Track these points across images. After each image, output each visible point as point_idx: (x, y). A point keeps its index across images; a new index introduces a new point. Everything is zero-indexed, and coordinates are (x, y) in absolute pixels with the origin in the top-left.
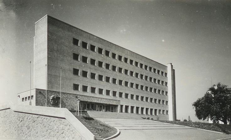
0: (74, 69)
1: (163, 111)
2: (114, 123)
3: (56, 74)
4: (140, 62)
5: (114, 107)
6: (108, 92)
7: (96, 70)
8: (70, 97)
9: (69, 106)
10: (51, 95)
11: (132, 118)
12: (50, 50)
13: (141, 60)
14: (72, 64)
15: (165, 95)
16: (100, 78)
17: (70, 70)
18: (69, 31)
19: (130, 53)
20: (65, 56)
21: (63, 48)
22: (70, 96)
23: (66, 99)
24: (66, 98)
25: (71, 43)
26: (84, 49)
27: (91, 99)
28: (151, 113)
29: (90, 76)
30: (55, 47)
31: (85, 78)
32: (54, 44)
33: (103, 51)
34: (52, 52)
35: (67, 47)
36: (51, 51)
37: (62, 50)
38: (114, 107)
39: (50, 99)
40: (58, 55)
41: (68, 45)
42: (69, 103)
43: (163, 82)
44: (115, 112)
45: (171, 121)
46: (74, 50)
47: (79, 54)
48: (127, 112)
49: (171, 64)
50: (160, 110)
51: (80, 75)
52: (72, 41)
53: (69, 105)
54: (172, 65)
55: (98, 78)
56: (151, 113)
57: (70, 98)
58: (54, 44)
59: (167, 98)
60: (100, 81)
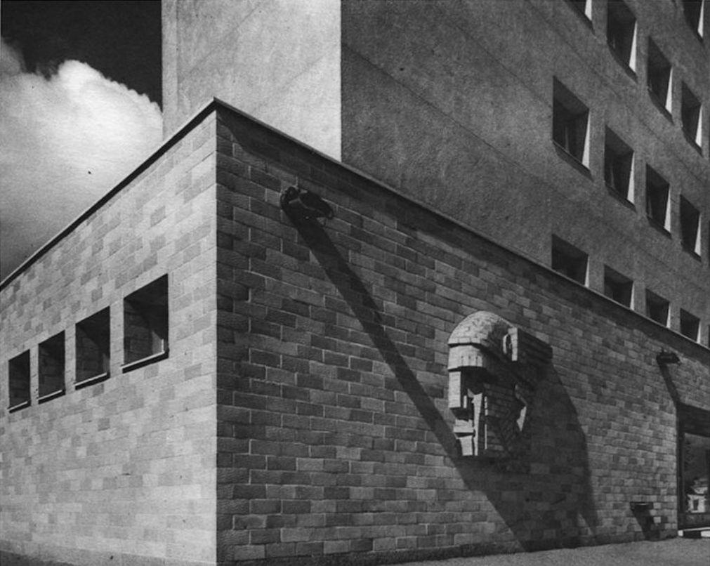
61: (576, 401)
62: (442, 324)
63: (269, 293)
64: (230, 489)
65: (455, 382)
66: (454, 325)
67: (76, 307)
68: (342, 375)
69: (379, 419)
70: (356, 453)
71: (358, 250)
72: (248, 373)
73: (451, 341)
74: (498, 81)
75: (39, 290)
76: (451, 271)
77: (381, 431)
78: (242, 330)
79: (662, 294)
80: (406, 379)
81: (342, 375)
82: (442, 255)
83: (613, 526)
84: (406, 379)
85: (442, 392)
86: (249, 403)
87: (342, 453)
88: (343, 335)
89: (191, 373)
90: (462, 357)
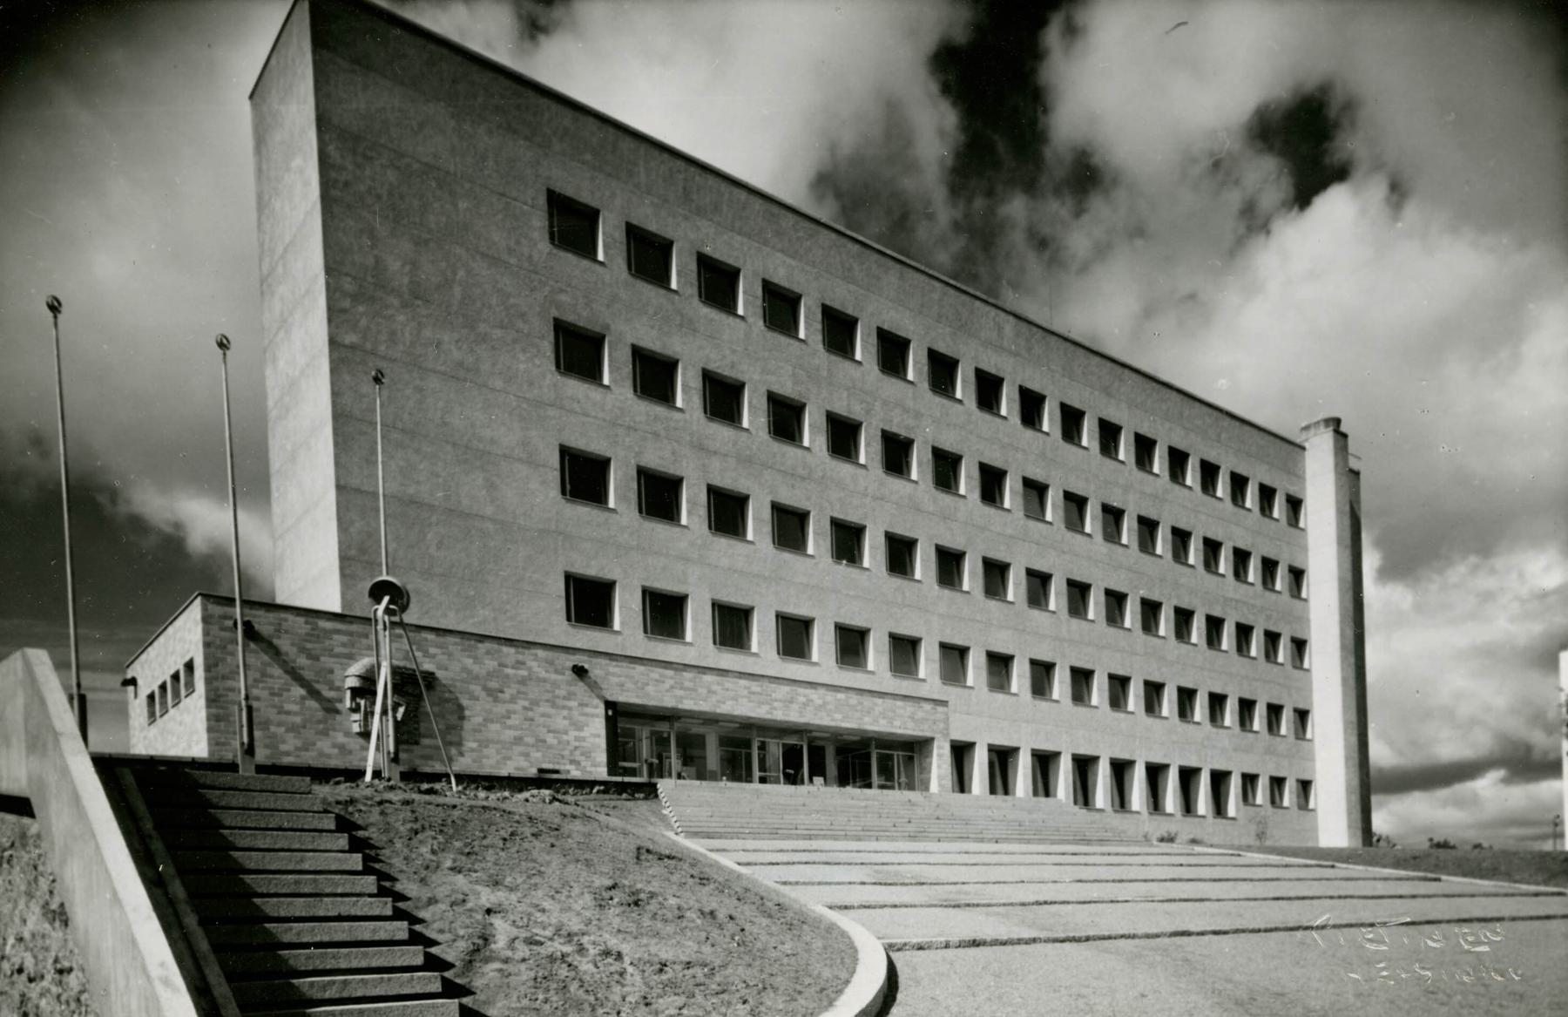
0: (565, 452)
1: (1277, 783)
2: (722, 825)
3: (411, 490)
4: (1095, 407)
5: (898, 755)
6: (851, 643)
7: (747, 461)
8: (525, 673)
9: (518, 749)
10: (351, 657)
11: (1025, 834)
12: (348, 285)
13: (1107, 391)
14: (551, 412)
15: (1289, 667)
16: (847, 540)
17: (532, 462)
18: (515, 132)
19: (1018, 335)
20: (484, 338)
21: (461, 273)
22: (519, 664)
23: (490, 692)
24: (493, 684)
25: (536, 235)
26: (648, 291)
27: (703, 691)
28: (1188, 807)
29: (703, 512)
30: (394, 265)
31: (659, 530)
32: (382, 230)
33: (1190, 467)
34: (372, 299)
35: (495, 261)
36: (356, 298)
37: (457, 291)
38: (898, 755)
39: (339, 689)
40: (427, 333)
41: (510, 251)
42: (515, 720)
43: (1269, 566)
44: (911, 786)
45: (1341, 850)
46: (563, 298)
47: (608, 327)
48: (1047, 794)
49: (1337, 422)
50: (1249, 780)
51: (618, 499)
52: (538, 221)
53: (518, 741)
54: (1343, 428)
55: (767, 528)
56: (1188, 807)
57: (523, 682)
58: (382, 230)
59: (1307, 689)
60: (787, 556)
61: (465, 702)
62: (338, 666)
63: (554, 422)
64: (213, 742)
65: (348, 694)
66: (351, 662)
67: (169, 668)
68: (273, 694)
69: (296, 714)
70: (282, 729)
71: (279, 637)
72: (219, 696)
73: (346, 674)
74: (666, 329)
75: (157, 656)
76: (345, 639)
77: (298, 720)
78: (216, 679)
79: (1077, 404)
80: (314, 693)
81: (273, 694)
82: (338, 632)
83: (654, 780)
84: (314, 693)
85: (341, 701)
86: (222, 708)
87: (273, 729)
88: (272, 676)
89: (200, 697)
90: (352, 682)
